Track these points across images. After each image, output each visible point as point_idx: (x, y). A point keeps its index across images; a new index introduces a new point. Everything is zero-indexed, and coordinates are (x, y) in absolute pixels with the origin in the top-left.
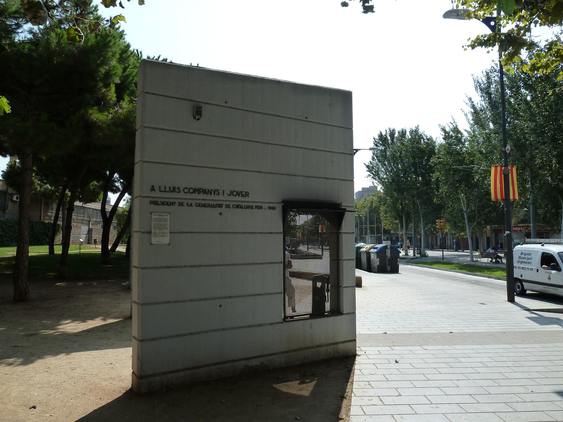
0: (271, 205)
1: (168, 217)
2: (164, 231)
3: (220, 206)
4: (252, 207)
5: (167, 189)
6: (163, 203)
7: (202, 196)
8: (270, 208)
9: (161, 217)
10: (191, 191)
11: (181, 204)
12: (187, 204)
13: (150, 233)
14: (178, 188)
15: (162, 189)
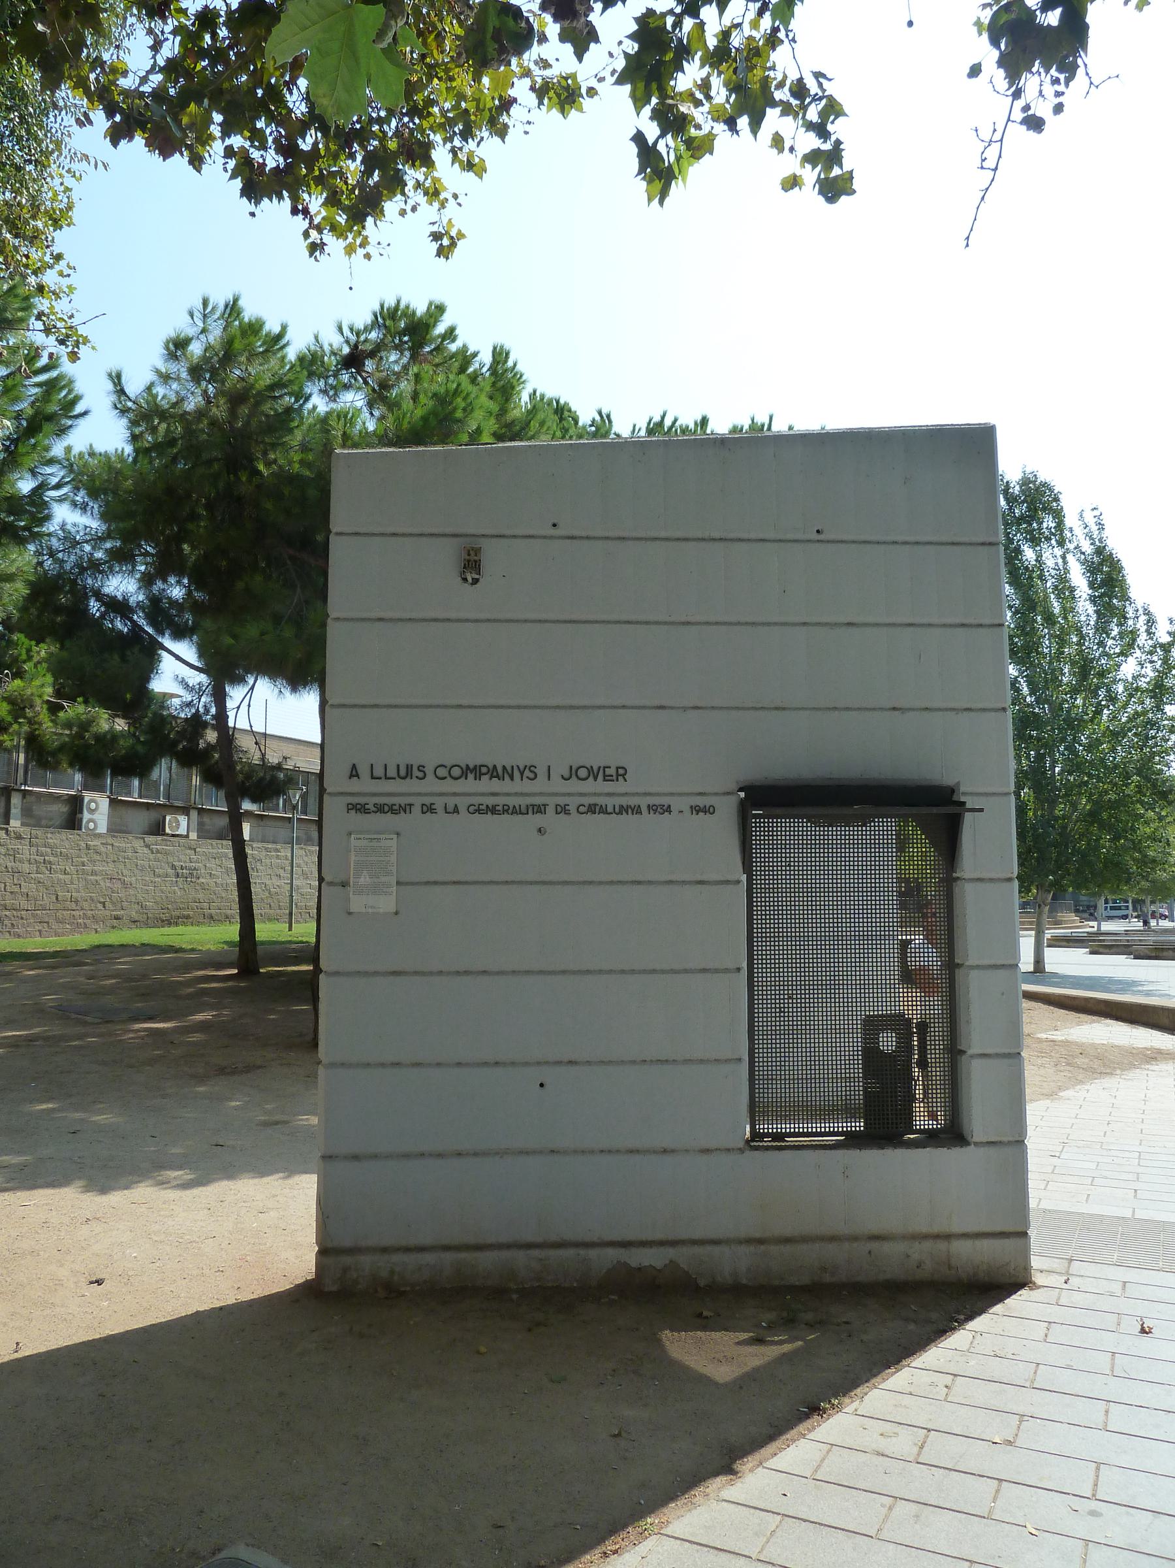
1: (393, 844)
5: (392, 772)
6: (380, 809)
9: (374, 844)
11: (429, 809)
14: (421, 768)
15: (379, 772)
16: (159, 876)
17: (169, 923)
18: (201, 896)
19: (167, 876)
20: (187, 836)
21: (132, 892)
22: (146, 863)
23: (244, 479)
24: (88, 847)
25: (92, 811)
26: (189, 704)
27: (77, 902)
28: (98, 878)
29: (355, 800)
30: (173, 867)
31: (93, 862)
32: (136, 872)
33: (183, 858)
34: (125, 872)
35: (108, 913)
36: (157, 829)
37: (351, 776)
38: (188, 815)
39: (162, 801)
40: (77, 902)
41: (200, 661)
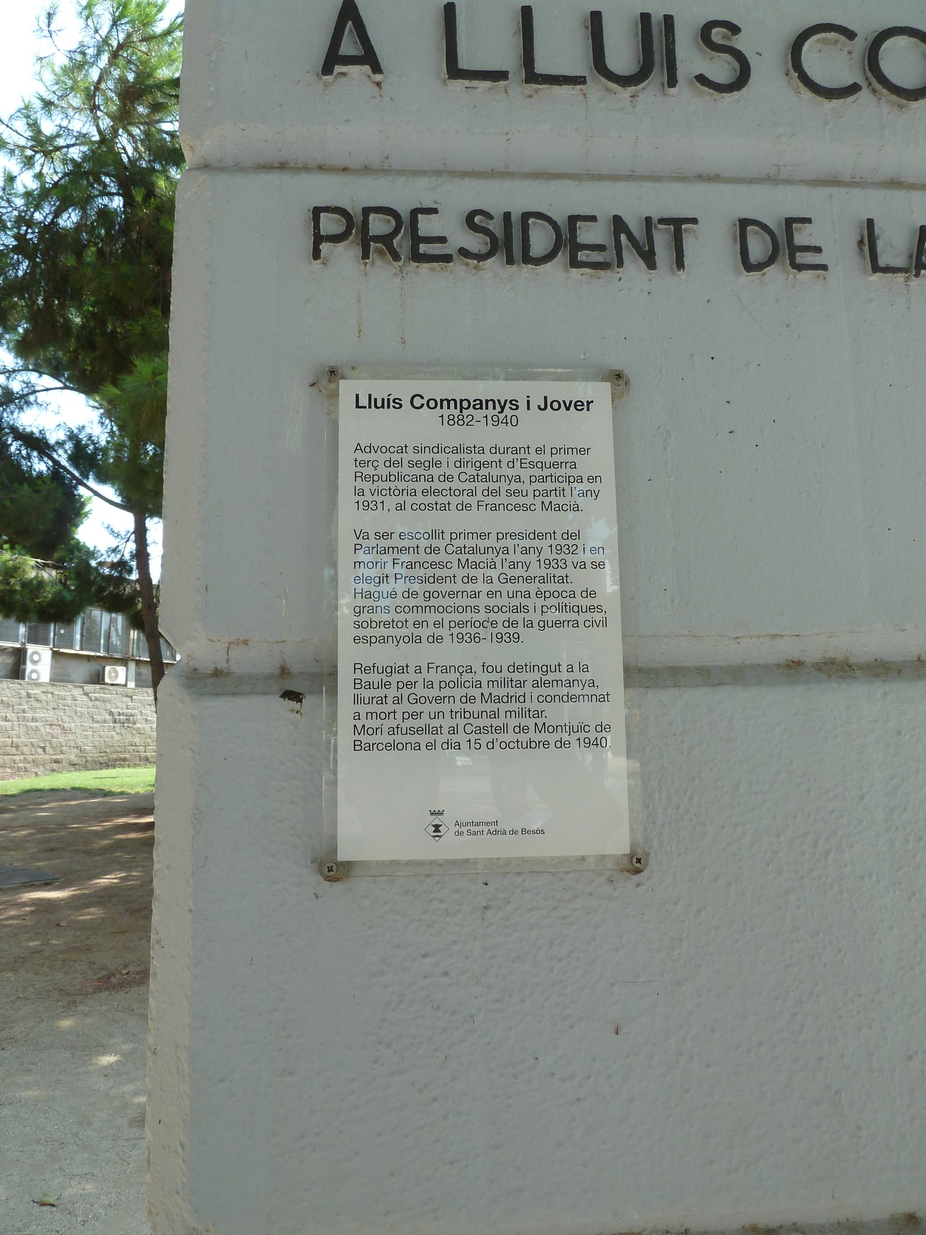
1: (595, 431)
2: (537, 647)
5: (561, 49)
6: (506, 240)
9: (481, 433)
11: (777, 246)
12: (869, 238)
14: (716, 35)
15: (488, 41)
16: (98, 722)
17: (107, 765)
18: (137, 740)
19: (105, 721)
20: (125, 685)
21: (71, 737)
22: (85, 710)
23: (139, 199)
24: (29, 696)
25: (35, 663)
26: (115, 550)
27: (17, 747)
28: (38, 724)
29: (355, 194)
30: (111, 713)
31: (33, 709)
32: (76, 718)
33: (120, 705)
34: (65, 719)
35: (47, 757)
36: (98, 678)
37: (333, 60)
38: (126, 665)
39: (102, 653)
40: (17, 747)
41: (120, 498)
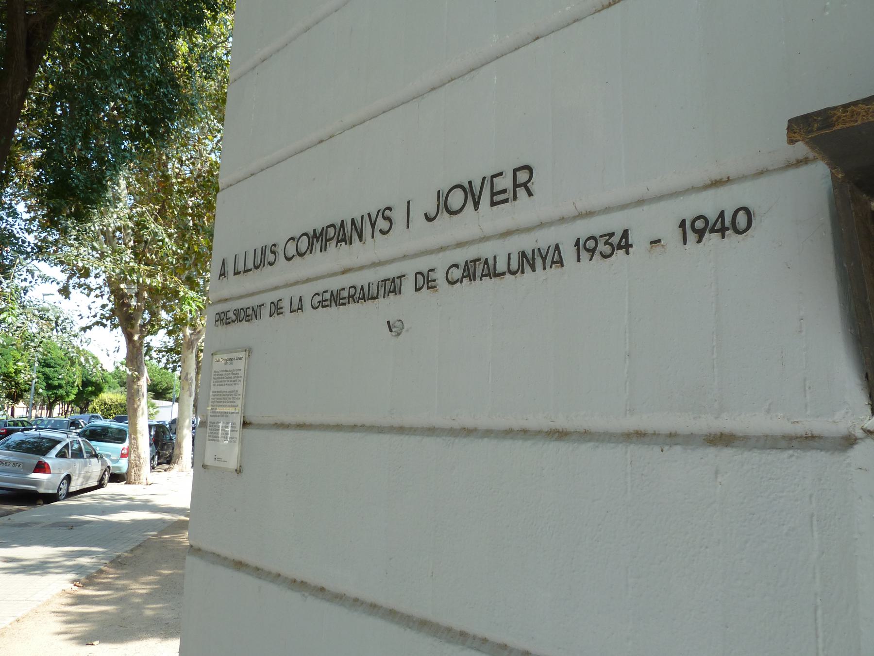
0: (708, 204)
3: (392, 287)
4: (553, 258)
7: (336, 257)
8: (698, 229)
10: (304, 243)
11: (276, 309)
13: (245, 424)
